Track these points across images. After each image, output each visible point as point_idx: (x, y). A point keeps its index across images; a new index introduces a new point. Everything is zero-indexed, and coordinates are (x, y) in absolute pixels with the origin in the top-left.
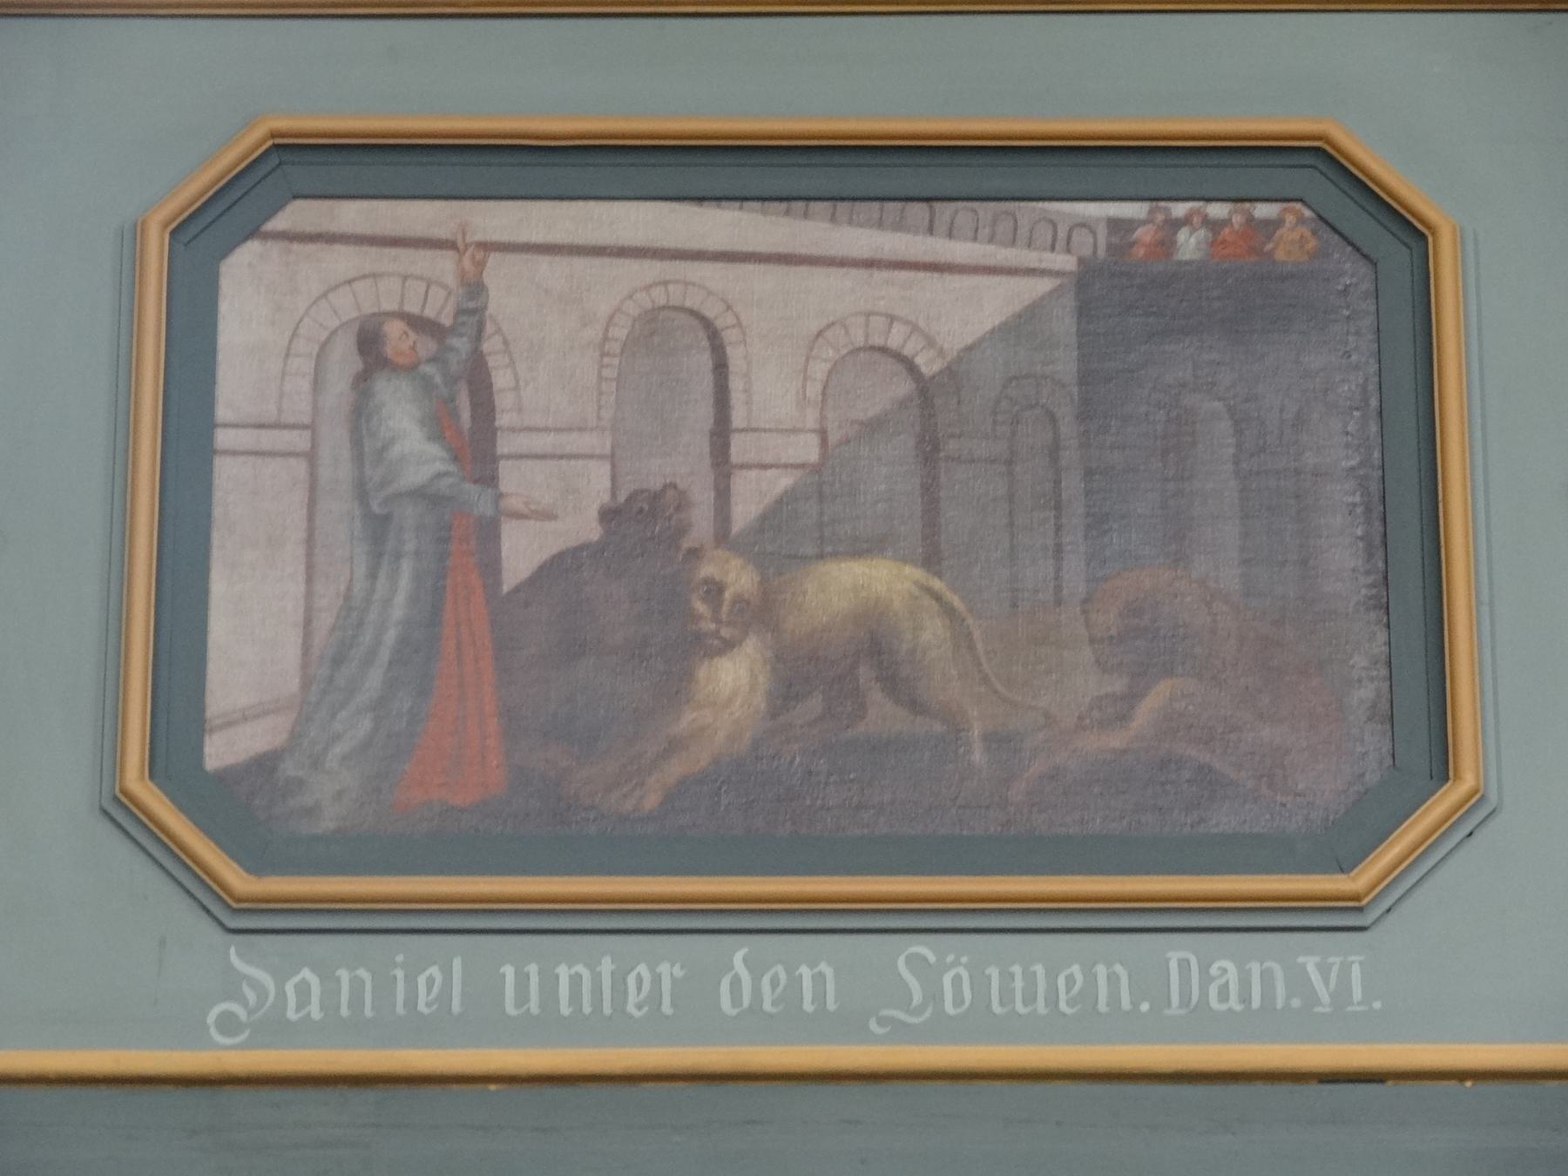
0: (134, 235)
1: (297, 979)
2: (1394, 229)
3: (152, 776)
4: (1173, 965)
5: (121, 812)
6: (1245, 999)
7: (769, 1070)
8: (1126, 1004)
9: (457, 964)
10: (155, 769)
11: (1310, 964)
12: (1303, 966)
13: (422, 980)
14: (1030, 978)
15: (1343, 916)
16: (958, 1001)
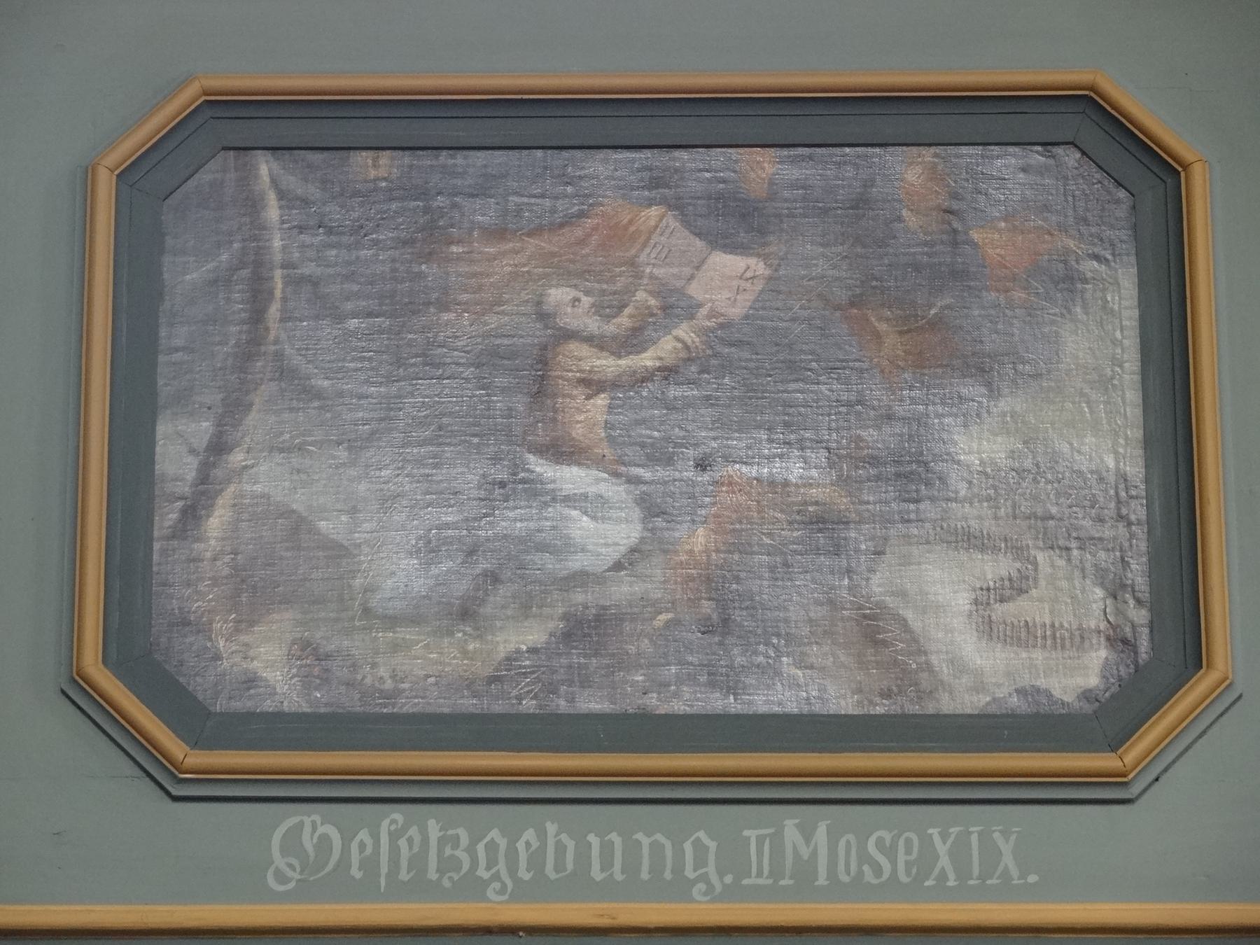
0: (88, 175)
1: (485, 841)
3: (105, 662)
5: (79, 694)
7: (163, 926)
11: (934, 832)
12: (931, 835)
13: (688, 847)
14: (607, 848)
15: (1110, 791)
16: (559, 866)
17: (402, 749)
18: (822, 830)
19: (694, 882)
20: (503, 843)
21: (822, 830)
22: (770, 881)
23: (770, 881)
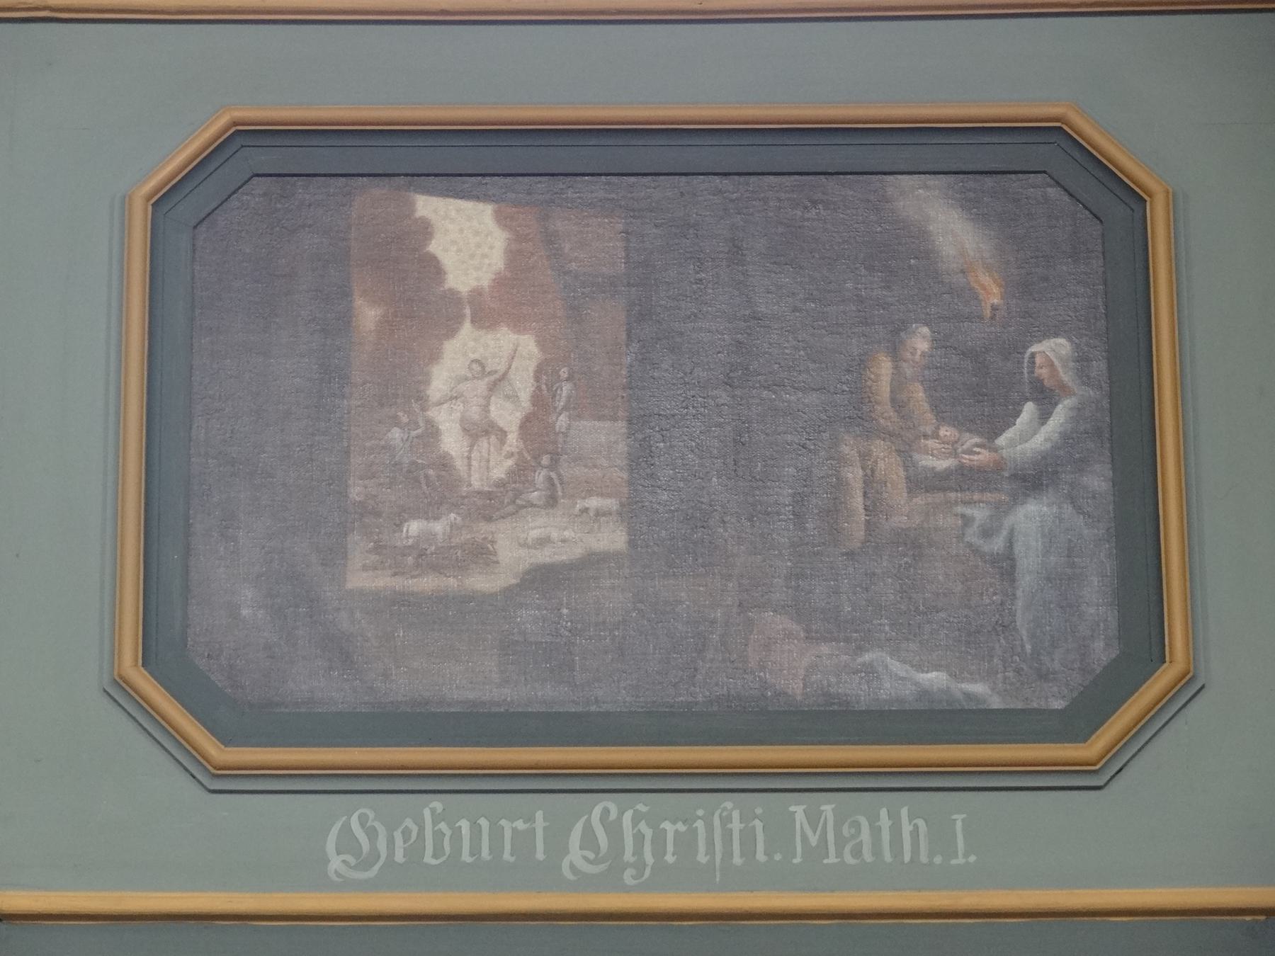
5: (120, 691)
8: (924, 858)
9: (884, 813)
10: (148, 659)
17: (761, 743)
20: (736, 826)
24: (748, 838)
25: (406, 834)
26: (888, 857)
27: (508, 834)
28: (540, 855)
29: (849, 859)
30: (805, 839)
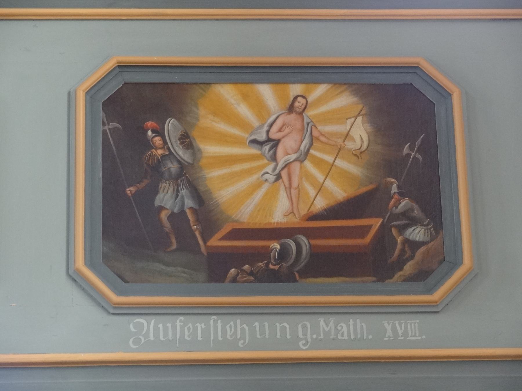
2: (137, 71)
4: (409, 325)
6: (349, 335)
9: (351, 320)
18: (332, 324)
19: (301, 339)
21: (332, 324)
22: (420, 338)
23: (420, 338)
24: (156, 330)
25: (189, 329)
26: (352, 337)
27: (199, 329)
28: (200, 338)
29: (339, 337)
30: (324, 329)
